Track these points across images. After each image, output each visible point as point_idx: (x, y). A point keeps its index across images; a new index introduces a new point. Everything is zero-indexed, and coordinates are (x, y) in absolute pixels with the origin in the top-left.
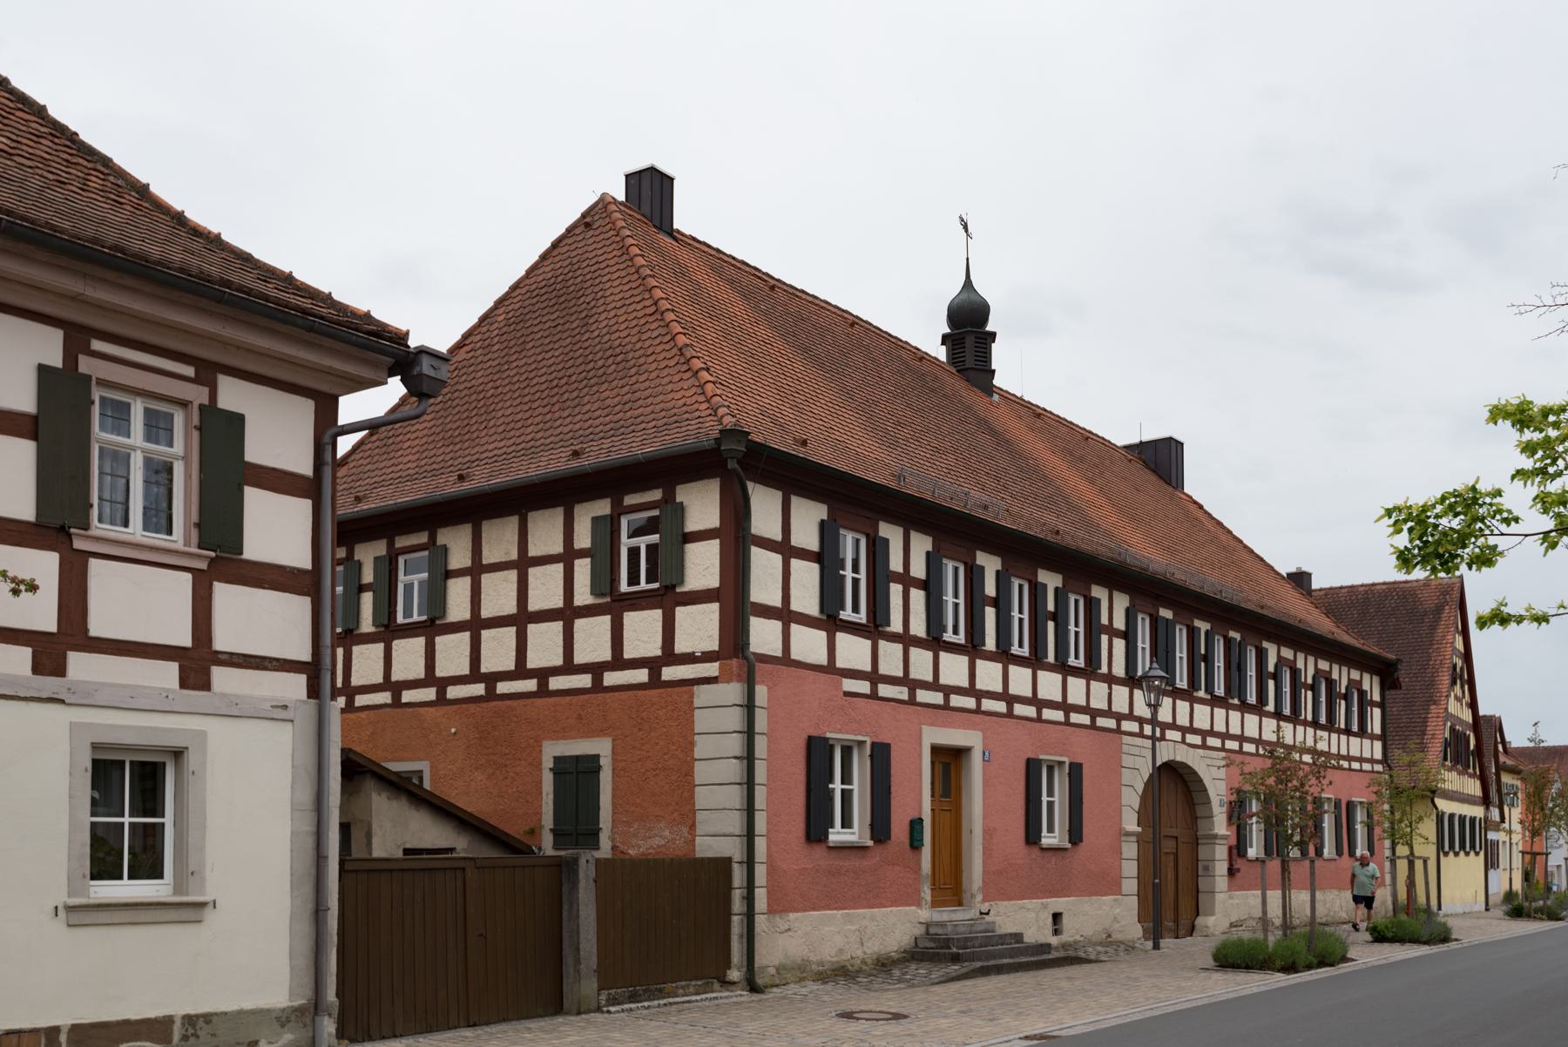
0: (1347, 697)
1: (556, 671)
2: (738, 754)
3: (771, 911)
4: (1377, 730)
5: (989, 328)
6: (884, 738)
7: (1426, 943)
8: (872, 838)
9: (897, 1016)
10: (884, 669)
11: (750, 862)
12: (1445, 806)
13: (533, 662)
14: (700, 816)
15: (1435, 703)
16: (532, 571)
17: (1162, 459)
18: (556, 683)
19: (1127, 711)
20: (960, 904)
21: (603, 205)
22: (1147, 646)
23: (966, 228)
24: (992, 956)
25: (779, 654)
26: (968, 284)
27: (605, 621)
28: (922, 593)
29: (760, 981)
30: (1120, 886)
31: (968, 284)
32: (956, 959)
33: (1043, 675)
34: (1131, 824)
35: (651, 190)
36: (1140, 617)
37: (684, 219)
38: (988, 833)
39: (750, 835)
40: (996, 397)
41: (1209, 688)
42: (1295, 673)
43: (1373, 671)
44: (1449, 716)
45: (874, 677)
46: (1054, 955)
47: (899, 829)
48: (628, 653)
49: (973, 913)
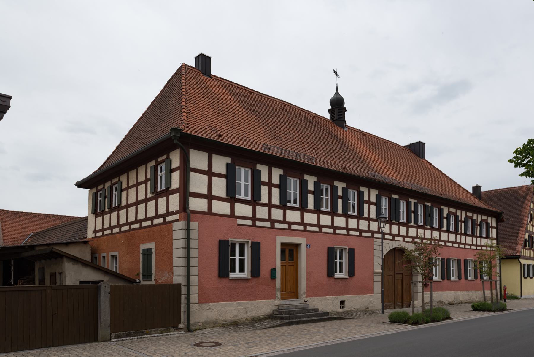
0: (480, 225)
1: (387, 234)
2: (184, 247)
3: (201, 302)
4: (494, 236)
6: (257, 240)
7: (494, 311)
8: (252, 276)
9: (218, 344)
10: (258, 216)
11: (188, 285)
12: (523, 261)
14: (174, 269)
15: (522, 227)
17: (417, 149)
18: (364, 234)
19: (455, 241)
20: (297, 298)
21: (184, 67)
22: (437, 217)
23: (336, 74)
24: (300, 317)
25: (206, 210)
26: (337, 92)
28: (313, 195)
29: (192, 328)
30: (373, 291)
31: (337, 92)
32: (282, 319)
33: (361, 222)
34: (378, 269)
35: (204, 61)
36: (435, 209)
37: (214, 71)
38: (308, 273)
39: (188, 276)
40: (346, 129)
41: (416, 221)
42: (456, 217)
43: (492, 216)
44: (527, 231)
45: (347, 229)
46: (330, 316)
47: (265, 271)
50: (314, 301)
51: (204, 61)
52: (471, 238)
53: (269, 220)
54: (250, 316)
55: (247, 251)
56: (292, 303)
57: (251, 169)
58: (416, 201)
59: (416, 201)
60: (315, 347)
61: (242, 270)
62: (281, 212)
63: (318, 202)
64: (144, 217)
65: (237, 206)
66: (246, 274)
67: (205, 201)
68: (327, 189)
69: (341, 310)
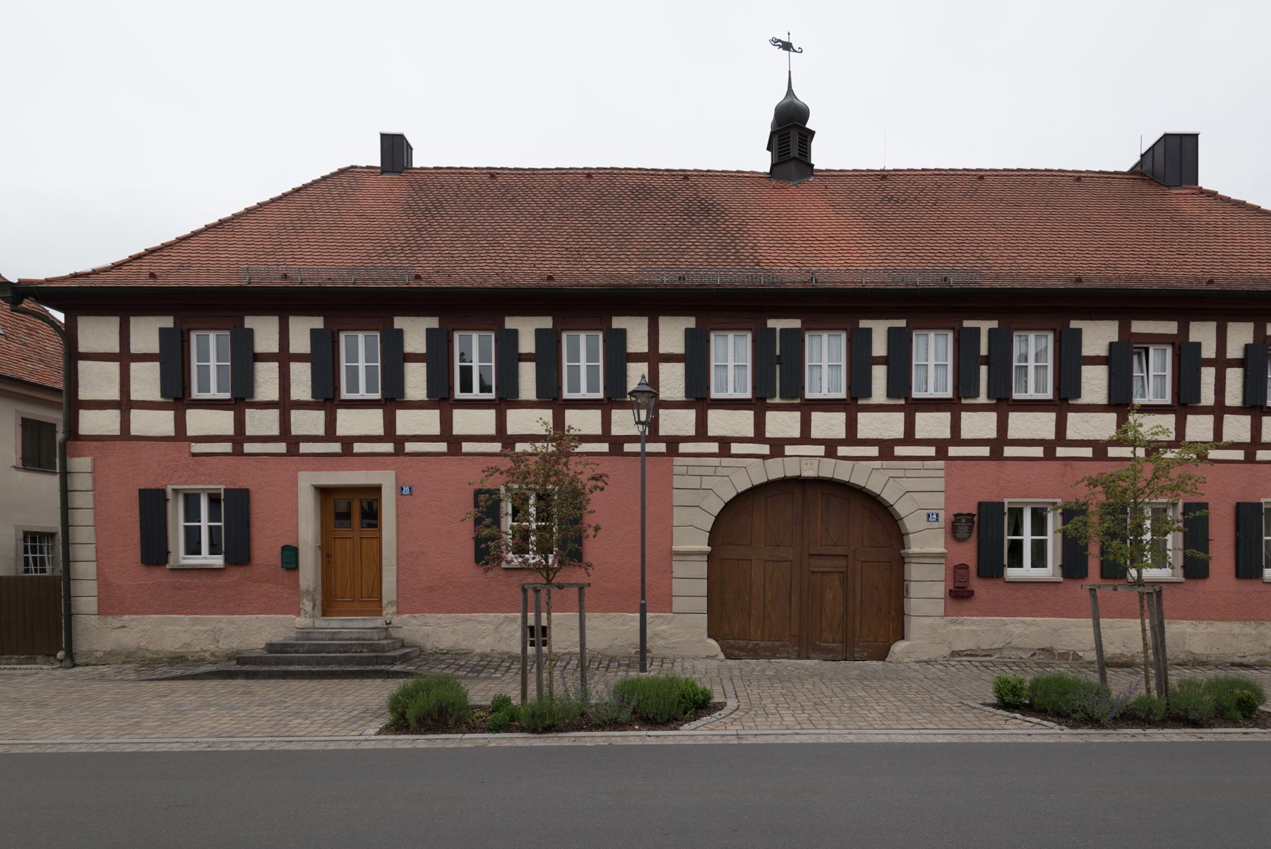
1: (1170, 445)
3: (103, 611)
5: (809, 125)
7: (1196, 724)
26: (790, 91)
31: (790, 91)
47: (265, 548)
49: (379, 622)
50: (425, 624)
51: (395, 148)
53: (606, 436)
54: (224, 647)
55: (1053, 522)
56: (349, 625)
57: (1054, 330)
58: (994, 324)
59: (994, 324)
61: (1039, 560)
62: (1246, 420)
63: (899, 383)
65: (458, 415)
66: (1050, 571)
67: (115, 415)
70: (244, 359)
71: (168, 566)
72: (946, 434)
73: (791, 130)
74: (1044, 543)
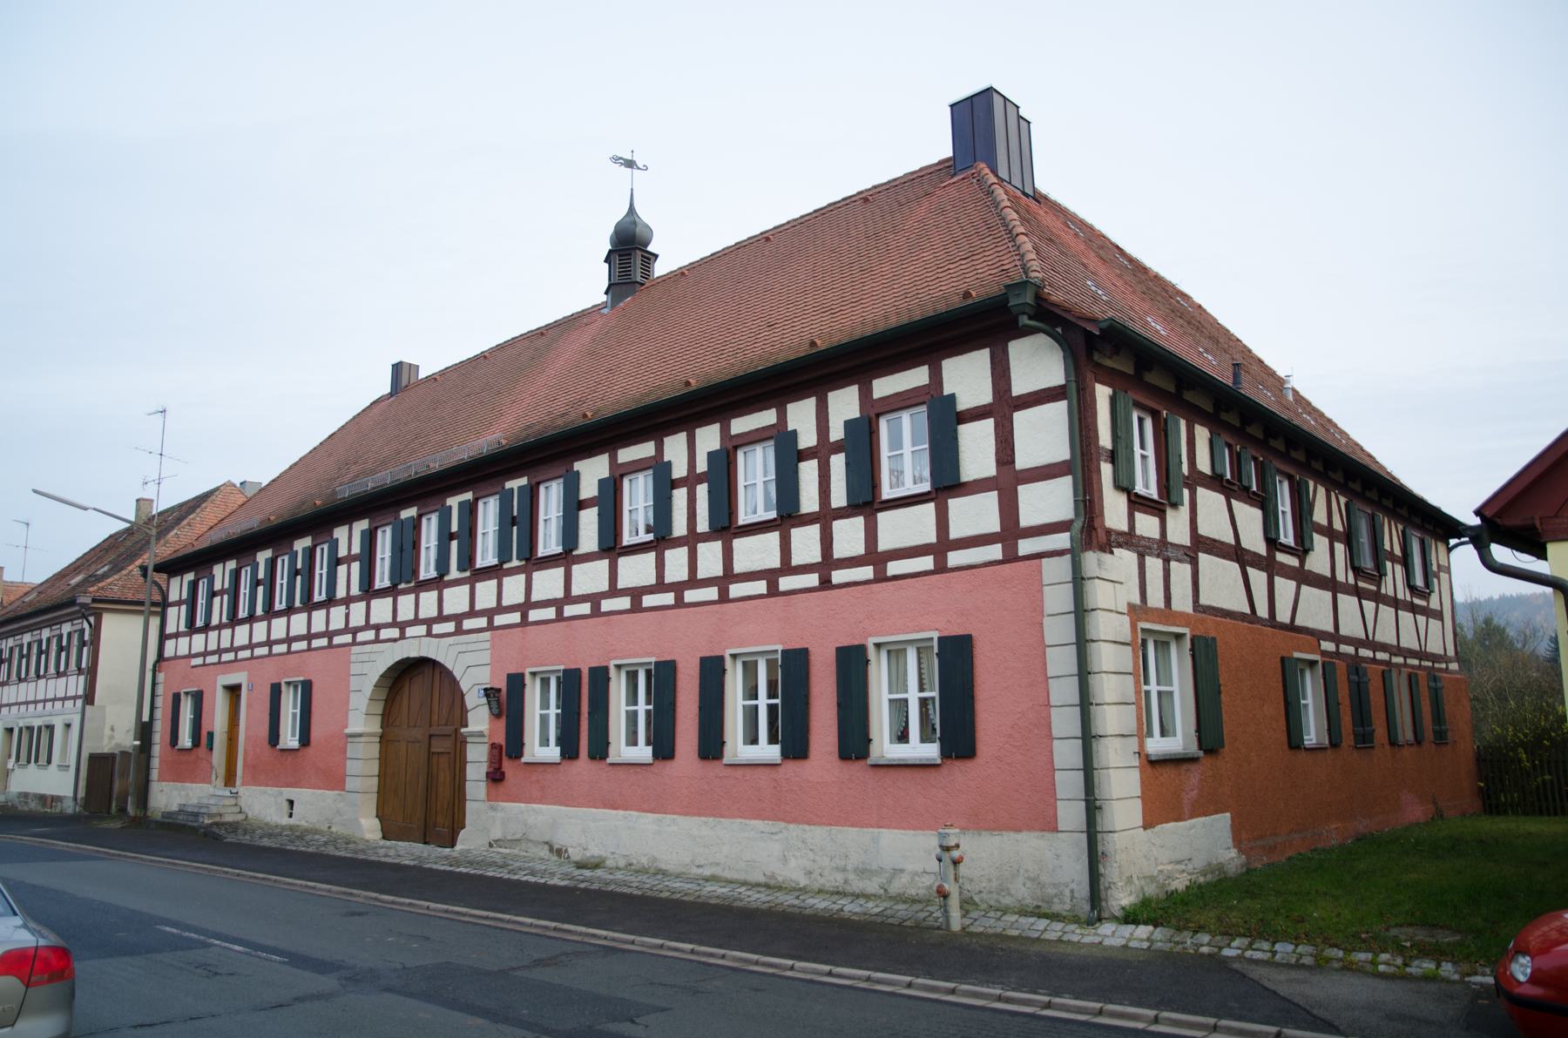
1: (650, 590)
13: (669, 578)
16: (1020, 418)
18: (649, 601)
26: (632, 210)
27: (859, 521)
31: (632, 210)
48: (701, 575)
52: (1293, 584)
60: (850, 908)
64: (435, 614)
67: (718, 571)
68: (1141, 420)
69: (285, 821)
70: (945, 420)
71: (869, 762)
72: (775, 562)
73: (629, 247)
74: (635, 713)
